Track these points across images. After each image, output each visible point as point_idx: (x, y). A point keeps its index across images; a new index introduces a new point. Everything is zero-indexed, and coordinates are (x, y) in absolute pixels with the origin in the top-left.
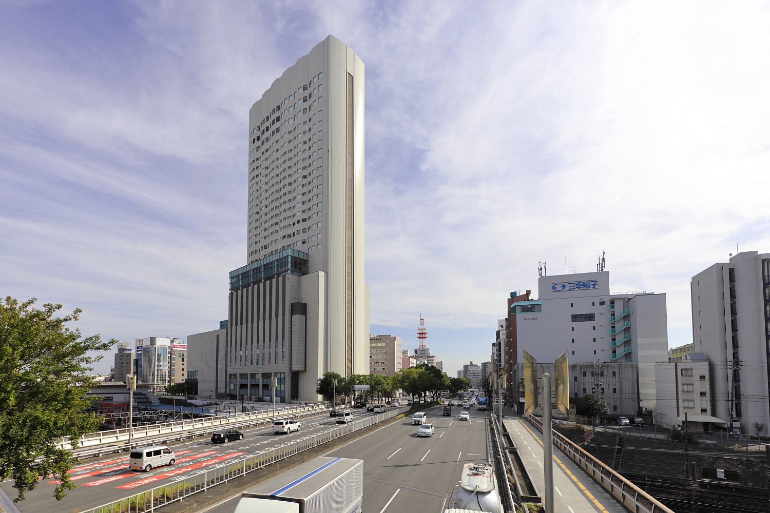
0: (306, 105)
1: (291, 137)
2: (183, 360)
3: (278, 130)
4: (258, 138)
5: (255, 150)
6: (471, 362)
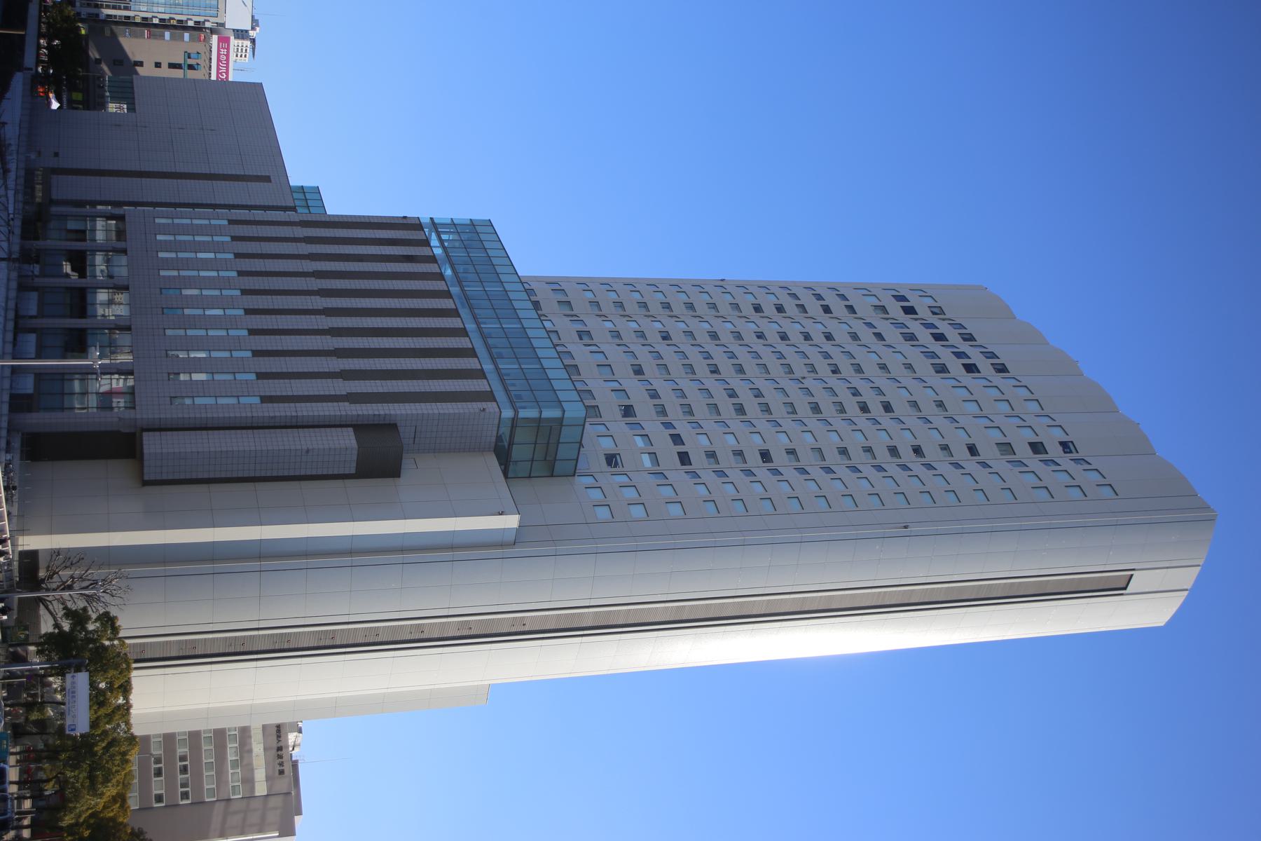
0: (1024, 452)
1: (929, 409)
4: (909, 310)
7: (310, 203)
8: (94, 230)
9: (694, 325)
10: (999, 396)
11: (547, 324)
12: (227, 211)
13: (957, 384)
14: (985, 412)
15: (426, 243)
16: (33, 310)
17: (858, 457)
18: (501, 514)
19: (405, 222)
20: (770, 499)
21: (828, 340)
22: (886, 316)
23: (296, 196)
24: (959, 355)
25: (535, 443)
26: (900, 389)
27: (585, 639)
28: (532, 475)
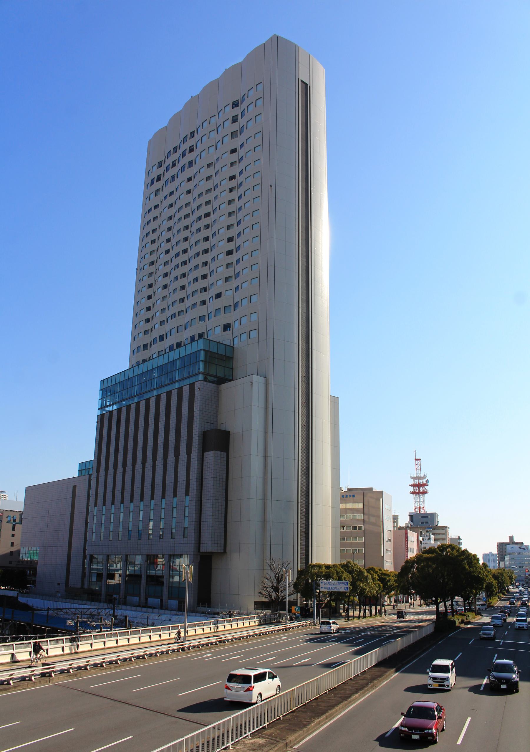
0: (236, 127)
1: (210, 171)
2: (14, 529)
3: (191, 164)
4: (159, 178)
5: (153, 195)
6: (511, 538)
7: (87, 467)
8: (97, 569)
9: (160, 262)
10: (206, 152)
11: (155, 356)
12: (90, 507)
13: (199, 157)
14: (215, 144)
15: (111, 413)
16: (136, 599)
17: (233, 207)
18: (252, 383)
19: (99, 422)
20: (251, 266)
21: (173, 206)
22: (161, 190)
23: (83, 474)
24: (184, 155)
25: (217, 364)
26: (203, 127)
27: (313, 545)
28: (232, 367)
